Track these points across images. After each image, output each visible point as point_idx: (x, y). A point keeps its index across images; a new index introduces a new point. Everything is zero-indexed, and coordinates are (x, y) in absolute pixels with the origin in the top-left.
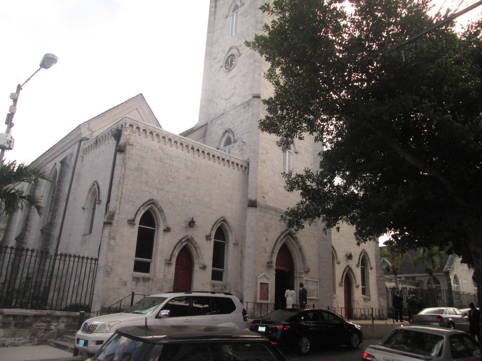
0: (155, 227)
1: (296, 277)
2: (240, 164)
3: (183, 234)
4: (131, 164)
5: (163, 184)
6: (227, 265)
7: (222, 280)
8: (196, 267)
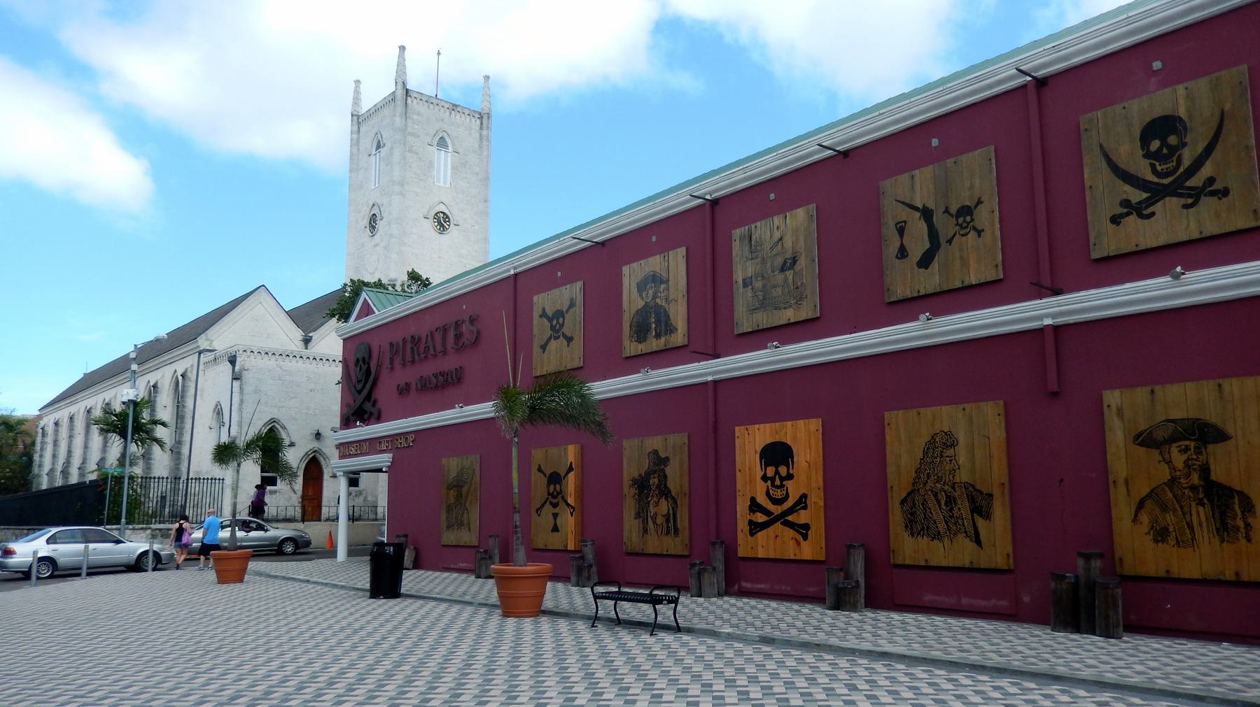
4: (248, 389)
8: (326, 477)
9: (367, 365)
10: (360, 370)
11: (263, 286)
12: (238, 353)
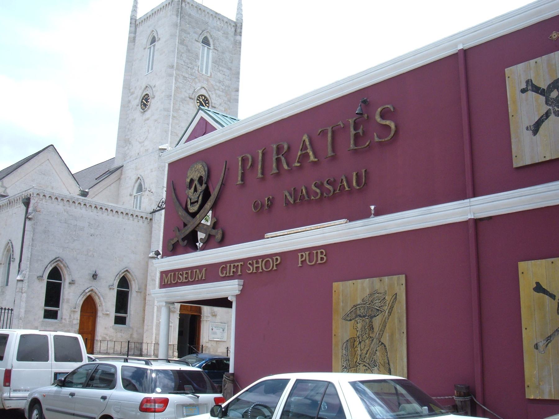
0: (61, 280)
1: (203, 320)
2: (145, 216)
3: (87, 285)
5: (68, 242)
6: (130, 310)
7: (125, 324)
9: (204, 186)
10: (195, 190)
11: (52, 145)
12: (32, 195)
